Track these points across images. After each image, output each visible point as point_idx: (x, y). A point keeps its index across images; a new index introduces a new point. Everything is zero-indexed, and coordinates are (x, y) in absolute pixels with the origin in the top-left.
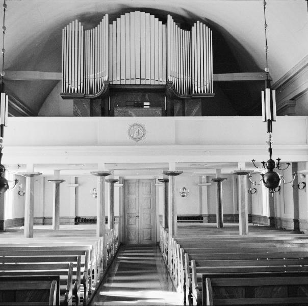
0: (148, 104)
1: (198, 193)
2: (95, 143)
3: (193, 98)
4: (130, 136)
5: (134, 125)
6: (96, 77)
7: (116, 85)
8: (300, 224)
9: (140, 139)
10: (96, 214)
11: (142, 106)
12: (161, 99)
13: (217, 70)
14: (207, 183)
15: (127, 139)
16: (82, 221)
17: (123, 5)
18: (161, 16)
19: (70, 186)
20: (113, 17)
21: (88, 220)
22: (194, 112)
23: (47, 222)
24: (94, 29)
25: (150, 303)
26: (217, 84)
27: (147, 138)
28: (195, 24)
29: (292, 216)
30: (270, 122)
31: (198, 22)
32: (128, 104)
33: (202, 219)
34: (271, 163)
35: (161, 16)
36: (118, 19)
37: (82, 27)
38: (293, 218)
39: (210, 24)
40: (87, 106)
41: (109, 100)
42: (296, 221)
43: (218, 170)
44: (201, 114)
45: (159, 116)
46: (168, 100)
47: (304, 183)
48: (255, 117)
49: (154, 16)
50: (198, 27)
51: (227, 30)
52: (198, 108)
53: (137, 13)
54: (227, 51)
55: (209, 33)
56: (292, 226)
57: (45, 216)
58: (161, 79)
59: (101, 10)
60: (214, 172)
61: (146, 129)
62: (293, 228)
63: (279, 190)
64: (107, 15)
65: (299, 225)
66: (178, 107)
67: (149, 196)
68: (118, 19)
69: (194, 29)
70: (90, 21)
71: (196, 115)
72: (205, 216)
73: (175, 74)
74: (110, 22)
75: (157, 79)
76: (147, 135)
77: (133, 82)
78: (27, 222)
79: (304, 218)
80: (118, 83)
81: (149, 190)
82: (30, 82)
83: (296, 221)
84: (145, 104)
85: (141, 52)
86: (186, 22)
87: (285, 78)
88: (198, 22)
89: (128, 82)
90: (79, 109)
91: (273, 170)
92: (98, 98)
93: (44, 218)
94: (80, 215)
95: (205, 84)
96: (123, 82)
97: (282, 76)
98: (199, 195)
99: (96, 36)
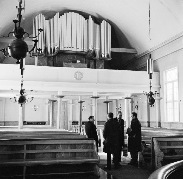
0: (80, 61)
1: (90, 109)
2: (57, 81)
3: (100, 60)
4: (75, 77)
5: (77, 72)
6: (51, 45)
7: (61, 50)
8: (150, 123)
9: (80, 79)
10: (46, 120)
11: (76, 62)
12: (83, 59)
13: (113, 46)
14: (73, 103)
15: (74, 79)
16: (27, 123)
17: (66, 8)
18: (86, 16)
19: (46, 105)
20: (61, 14)
21: (31, 123)
22: (101, 67)
23: (6, 124)
24: (51, 19)
25: (36, 164)
26: (112, 53)
27: (84, 79)
28: (102, 22)
29: (146, 120)
30: (151, 74)
31: (104, 20)
32: (69, 61)
33: (45, 123)
34: (151, 94)
35: (86, 16)
36: (63, 15)
37: (44, 18)
38: (147, 121)
39: (109, 22)
40: (46, 61)
41: (58, 58)
42: (149, 122)
43: (107, 97)
44: (94, 68)
45: (86, 68)
46: (89, 59)
47: (137, 106)
48: (117, 70)
49: (81, 15)
50: (103, 23)
51: (117, 25)
52: (102, 64)
53: (73, 13)
54: (118, 37)
55: (109, 27)
56: (147, 125)
57: (5, 121)
58: (84, 49)
59: (54, 9)
60: (105, 98)
61: (83, 75)
62: (147, 126)
63: (154, 106)
64: (58, 13)
65: (150, 124)
66: (92, 64)
67: (64, 111)
68: (63, 15)
69: (102, 24)
70: (49, 15)
71: (101, 68)
72: (47, 121)
73: (93, 48)
74: (61, 15)
75: (82, 49)
76: (83, 77)
77: (70, 49)
78: (79, 123)
79: (170, 120)
80: (63, 49)
81: (64, 107)
82: (18, 44)
83: (149, 122)
84: (78, 61)
85: (72, 35)
86: (98, 20)
87: (143, 54)
88: (104, 20)
89: (67, 49)
90: (41, 62)
91: (152, 96)
92: (52, 57)
93: (5, 122)
94: (25, 120)
95: (107, 53)
96: (65, 49)
97: (143, 52)
98: (90, 111)
99: (51, 24)
